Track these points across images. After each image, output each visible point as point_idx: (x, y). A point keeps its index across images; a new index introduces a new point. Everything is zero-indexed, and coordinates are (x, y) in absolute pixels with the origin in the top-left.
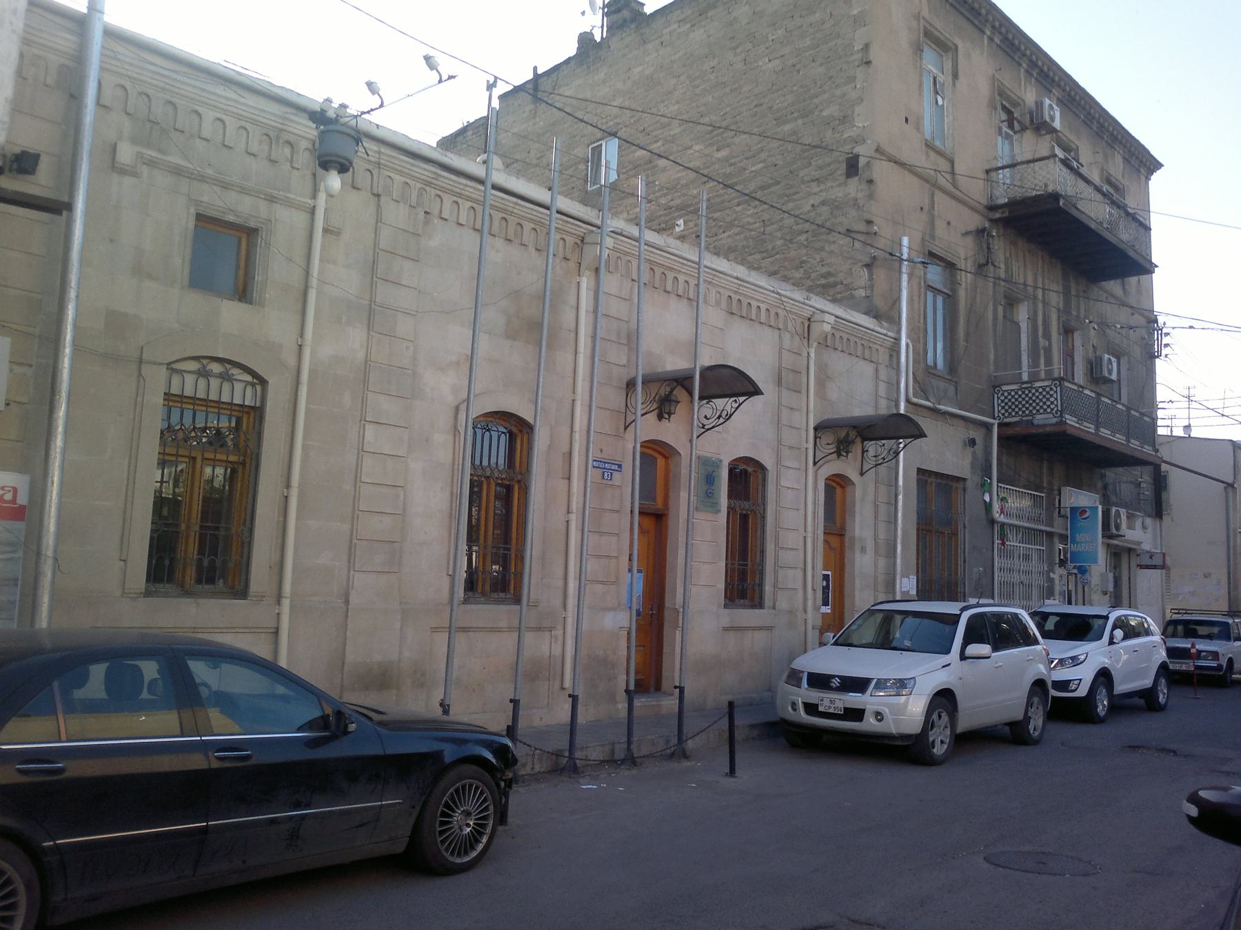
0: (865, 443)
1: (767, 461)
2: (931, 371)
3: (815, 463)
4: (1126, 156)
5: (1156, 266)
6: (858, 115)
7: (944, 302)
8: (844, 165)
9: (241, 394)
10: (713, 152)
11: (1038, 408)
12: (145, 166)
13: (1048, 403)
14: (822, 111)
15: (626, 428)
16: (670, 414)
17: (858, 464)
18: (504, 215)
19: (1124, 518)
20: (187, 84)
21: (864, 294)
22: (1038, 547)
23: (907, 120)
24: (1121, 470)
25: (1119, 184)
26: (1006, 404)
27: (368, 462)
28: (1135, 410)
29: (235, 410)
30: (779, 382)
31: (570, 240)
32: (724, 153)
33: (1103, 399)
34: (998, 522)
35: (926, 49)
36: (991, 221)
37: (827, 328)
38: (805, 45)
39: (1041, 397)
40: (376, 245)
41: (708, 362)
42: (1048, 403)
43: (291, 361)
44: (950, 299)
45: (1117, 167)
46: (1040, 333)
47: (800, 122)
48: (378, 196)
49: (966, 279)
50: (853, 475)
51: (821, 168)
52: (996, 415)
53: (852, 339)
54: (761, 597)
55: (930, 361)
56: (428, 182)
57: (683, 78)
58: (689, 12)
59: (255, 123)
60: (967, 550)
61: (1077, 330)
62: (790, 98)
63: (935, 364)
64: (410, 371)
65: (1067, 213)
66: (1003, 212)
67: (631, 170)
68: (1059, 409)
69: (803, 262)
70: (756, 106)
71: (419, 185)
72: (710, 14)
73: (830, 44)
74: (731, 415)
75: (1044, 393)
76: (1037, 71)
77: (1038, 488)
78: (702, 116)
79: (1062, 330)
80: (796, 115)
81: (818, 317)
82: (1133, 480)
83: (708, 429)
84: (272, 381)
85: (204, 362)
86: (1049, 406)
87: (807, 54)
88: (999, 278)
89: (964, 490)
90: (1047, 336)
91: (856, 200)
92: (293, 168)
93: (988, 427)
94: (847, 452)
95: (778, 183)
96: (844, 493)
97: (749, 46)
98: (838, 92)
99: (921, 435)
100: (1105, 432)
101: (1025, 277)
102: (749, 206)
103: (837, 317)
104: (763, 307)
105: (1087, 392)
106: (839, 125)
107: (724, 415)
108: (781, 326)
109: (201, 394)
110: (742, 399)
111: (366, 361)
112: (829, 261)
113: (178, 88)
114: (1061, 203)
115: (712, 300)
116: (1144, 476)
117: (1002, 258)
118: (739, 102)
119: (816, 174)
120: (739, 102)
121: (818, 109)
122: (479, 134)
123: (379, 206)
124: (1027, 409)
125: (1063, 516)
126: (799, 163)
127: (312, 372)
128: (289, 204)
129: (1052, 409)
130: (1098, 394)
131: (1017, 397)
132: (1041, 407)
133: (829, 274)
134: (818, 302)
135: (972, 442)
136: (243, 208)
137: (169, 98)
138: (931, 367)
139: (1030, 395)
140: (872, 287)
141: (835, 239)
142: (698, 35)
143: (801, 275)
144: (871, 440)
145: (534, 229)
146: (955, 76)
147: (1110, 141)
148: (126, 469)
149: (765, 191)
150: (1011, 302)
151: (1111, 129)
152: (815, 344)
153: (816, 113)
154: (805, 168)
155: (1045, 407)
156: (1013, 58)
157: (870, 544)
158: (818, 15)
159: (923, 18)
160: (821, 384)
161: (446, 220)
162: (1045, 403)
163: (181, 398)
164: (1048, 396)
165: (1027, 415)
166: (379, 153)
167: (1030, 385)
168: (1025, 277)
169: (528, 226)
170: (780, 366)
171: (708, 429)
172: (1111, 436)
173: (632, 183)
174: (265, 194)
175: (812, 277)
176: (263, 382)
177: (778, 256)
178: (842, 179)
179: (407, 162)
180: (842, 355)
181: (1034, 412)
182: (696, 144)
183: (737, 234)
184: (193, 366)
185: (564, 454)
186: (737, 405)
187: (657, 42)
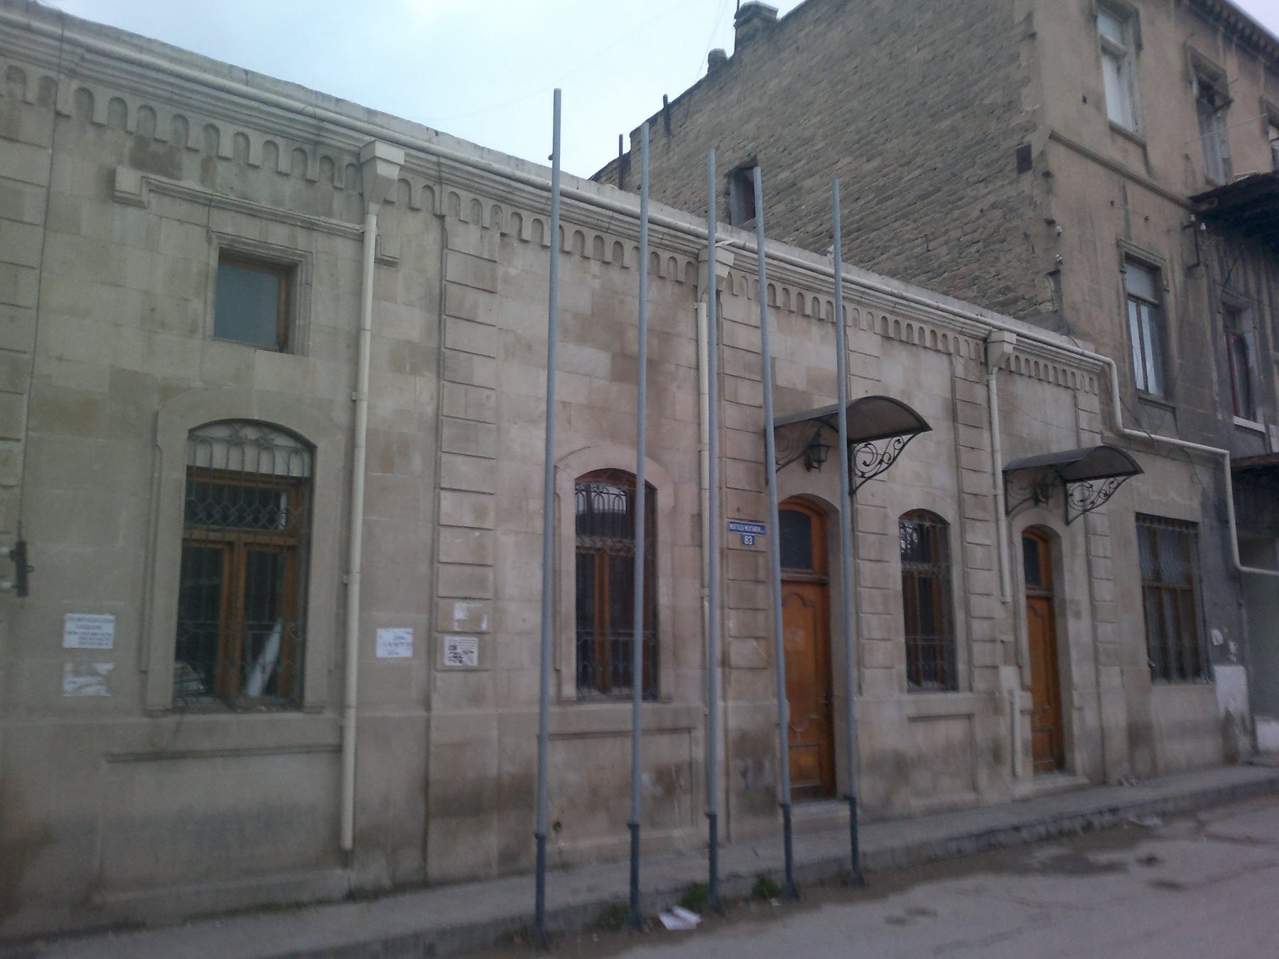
1: (949, 513)
2: (1143, 398)
3: (1007, 513)
6: (1026, 97)
7: (1150, 314)
9: (283, 464)
14: (982, 99)
16: (820, 462)
17: (1061, 512)
18: (598, 233)
21: (1051, 308)
23: (1085, 100)
30: (954, 416)
31: (682, 260)
32: (875, 163)
36: (1198, 215)
37: (1008, 349)
38: (959, 25)
40: (442, 277)
43: (341, 417)
44: (1157, 309)
47: (959, 115)
50: (1056, 525)
51: (987, 166)
53: (1042, 362)
55: (1140, 385)
56: (501, 196)
57: (823, 84)
58: (825, 8)
59: (283, 135)
63: (1146, 386)
64: (493, 426)
67: (774, 196)
69: (977, 278)
71: (492, 202)
74: (895, 459)
78: (847, 125)
80: (953, 108)
81: (996, 336)
83: (870, 478)
84: (322, 445)
91: (1033, 198)
92: (335, 188)
93: (1216, 461)
94: (1047, 498)
95: (939, 190)
99: (1136, 471)
101: (1246, 285)
102: (908, 220)
103: (1019, 335)
107: (886, 459)
110: (906, 438)
112: (1006, 273)
113: (179, 95)
115: (864, 325)
118: (888, 102)
120: (888, 102)
121: (979, 97)
122: (612, 179)
123: (443, 230)
128: (331, 232)
133: (1008, 289)
134: (995, 319)
136: (278, 238)
138: (1143, 392)
140: (1060, 298)
144: (1074, 481)
146: (1139, 46)
149: (926, 201)
150: (1233, 313)
152: (995, 370)
153: (977, 103)
154: (969, 168)
160: (1007, 415)
168: (1246, 285)
171: (870, 478)
173: (776, 211)
174: (303, 221)
175: (989, 294)
176: (310, 448)
177: (946, 275)
178: (1014, 175)
182: (843, 157)
183: (898, 254)
184: (222, 432)
186: (901, 445)
187: (794, 47)
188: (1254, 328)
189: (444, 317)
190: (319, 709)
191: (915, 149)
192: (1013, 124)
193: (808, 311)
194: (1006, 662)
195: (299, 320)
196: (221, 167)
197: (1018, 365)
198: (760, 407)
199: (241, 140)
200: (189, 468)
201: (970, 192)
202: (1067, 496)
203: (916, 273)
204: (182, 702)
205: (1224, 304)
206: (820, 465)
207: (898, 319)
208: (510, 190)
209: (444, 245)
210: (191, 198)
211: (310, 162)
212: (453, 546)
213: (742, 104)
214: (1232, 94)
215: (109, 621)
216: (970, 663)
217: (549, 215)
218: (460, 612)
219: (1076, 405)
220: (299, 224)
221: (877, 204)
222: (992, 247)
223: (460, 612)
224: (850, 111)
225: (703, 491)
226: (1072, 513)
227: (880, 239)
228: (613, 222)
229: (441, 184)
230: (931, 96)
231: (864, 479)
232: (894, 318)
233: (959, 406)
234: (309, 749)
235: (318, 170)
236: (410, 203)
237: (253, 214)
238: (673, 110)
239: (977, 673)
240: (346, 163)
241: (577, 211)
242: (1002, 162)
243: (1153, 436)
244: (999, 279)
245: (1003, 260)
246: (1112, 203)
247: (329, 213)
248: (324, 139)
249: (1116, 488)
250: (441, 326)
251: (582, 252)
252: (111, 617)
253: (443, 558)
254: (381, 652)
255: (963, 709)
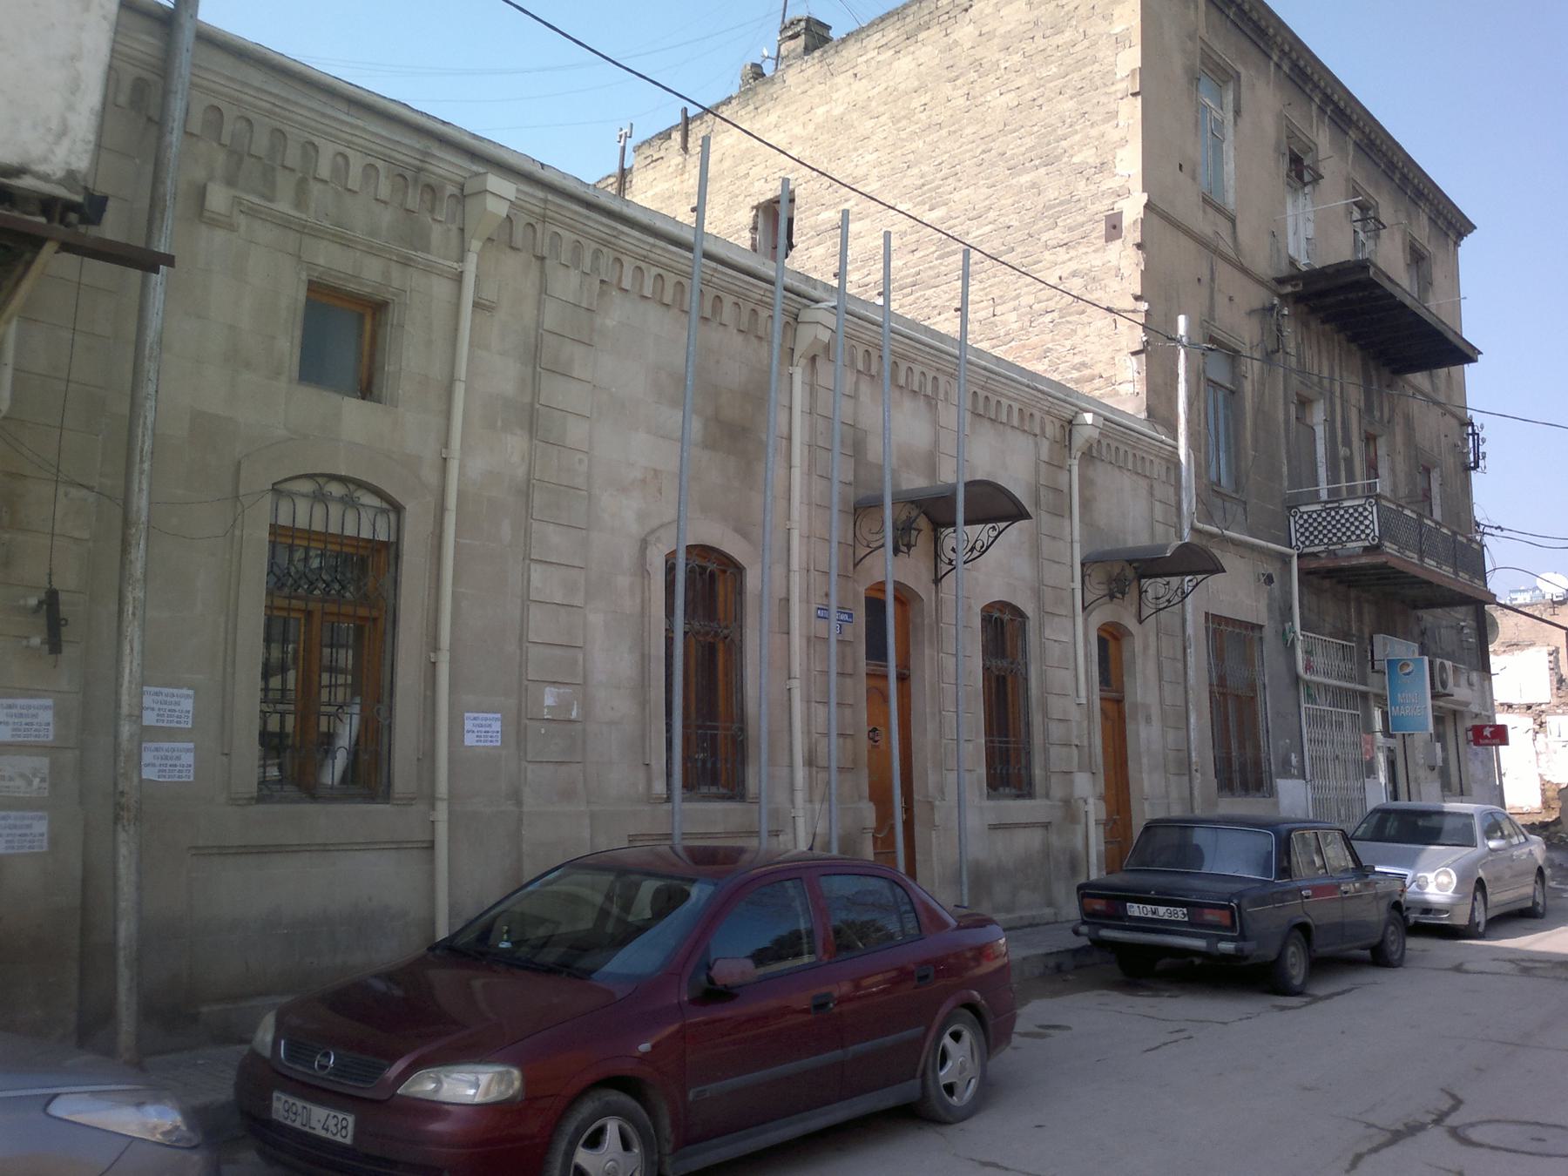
0: (1143, 581)
3: (1084, 608)
4: (1433, 216)
5: (1480, 353)
8: (1103, 225)
9: (366, 525)
10: (924, 212)
11: (1349, 533)
12: (242, 216)
13: (1362, 527)
14: (1072, 156)
15: (855, 565)
17: (1134, 609)
19: (1450, 672)
20: (303, 106)
22: (1354, 712)
24: (1439, 611)
25: (1426, 253)
26: (1307, 529)
27: (535, 614)
28: (1462, 535)
29: (346, 545)
33: (1426, 521)
34: (1304, 680)
35: (1204, 79)
36: (1280, 296)
39: (1352, 520)
40: (539, 324)
41: (968, 478)
42: (1362, 527)
43: (430, 475)
45: (1422, 231)
46: (1339, 439)
47: (1042, 170)
48: (542, 259)
49: (1252, 369)
50: (1130, 623)
51: (1071, 229)
52: (1294, 544)
54: (1030, 783)
57: (883, 119)
58: (893, 35)
59: (387, 159)
60: (1269, 715)
61: (1381, 436)
62: (1029, 141)
65: (1378, 286)
66: (1296, 285)
67: (812, 237)
68: (1377, 534)
69: (1049, 350)
70: (984, 152)
71: (594, 246)
72: (920, 37)
73: (1083, 71)
74: (988, 548)
75: (1356, 515)
76: (1332, 107)
77: (1346, 636)
79: (1363, 435)
82: (1454, 624)
84: (410, 507)
85: (321, 481)
86: (1363, 531)
87: (1051, 85)
88: (1291, 370)
89: (1261, 638)
90: (1347, 442)
93: (1285, 560)
95: (1013, 250)
96: (1120, 651)
97: (973, 75)
98: (1094, 132)
99: (1218, 569)
100: (1430, 563)
103: (1106, 419)
104: (1016, 406)
105: (1407, 512)
106: (1095, 173)
108: (1038, 431)
109: (318, 526)
110: (1002, 525)
111: (529, 481)
112: (1083, 348)
114: (1371, 273)
116: (1462, 615)
117: (1292, 345)
119: (1065, 237)
121: (1067, 155)
123: (542, 272)
124: (1335, 534)
125: (1377, 672)
126: (1041, 224)
127: (461, 495)
129: (1368, 535)
130: (1419, 515)
131: (1320, 520)
132: (1353, 533)
133: (1084, 365)
135: (1269, 579)
136: (370, 274)
137: (278, 125)
139: (1338, 517)
141: (1090, 320)
142: (905, 63)
143: (1045, 367)
144: (1150, 577)
145: (736, 304)
147: (1413, 196)
148: (531, 616)
150: (1304, 403)
151: (1416, 181)
155: (1358, 532)
156: (1304, 92)
157: (1155, 712)
158: (1067, 34)
159: (1201, 38)
160: (1086, 504)
161: (627, 291)
162: (1357, 527)
163: (293, 531)
164: (1361, 518)
165: (1334, 544)
166: (546, 201)
167: (1337, 505)
169: (728, 300)
170: (1037, 482)
172: (1437, 569)
175: (1061, 370)
176: (398, 509)
177: (1013, 343)
179: (580, 214)
180: (1109, 467)
181: (1344, 539)
184: (307, 487)
185: (780, 600)
186: (996, 533)
187: (851, 73)
188: (1326, 420)
189: (538, 369)
190: (410, 801)
191: (987, 202)
192: (1104, 187)
193: (902, 382)
194: (1081, 769)
195: (389, 365)
196: (315, 188)
197: (1099, 451)
198: (850, 484)
199: (340, 159)
200: (271, 525)
201: (1047, 255)
202: (1141, 592)
203: (979, 339)
204: (266, 792)
205: (1297, 394)
206: (909, 550)
207: (989, 395)
208: (615, 233)
209: (543, 289)
210: (285, 224)
211: (410, 191)
212: (541, 626)
213: (781, 130)
214: (1322, 171)
215: (188, 696)
216: (1046, 768)
217: (689, 276)
218: (550, 697)
219: (1152, 495)
220: (395, 258)
221: (937, 259)
222: (1068, 319)
223: (550, 697)
224: (913, 152)
225: (792, 574)
226: (1146, 612)
227: (939, 297)
228: (716, 274)
229: (544, 222)
230: (1011, 147)
231: (869, 550)
232: (985, 393)
233: (1043, 492)
234: (399, 846)
235: (418, 200)
236: (511, 241)
237: (346, 243)
238: (694, 124)
239: (1054, 779)
240: (448, 193)
241: (682, 261)
242: (1088, 227)
243: (1226, 532)
244: (1074, 354)
245: (1080, 333)
246: (1199, 280)
247: (427, 249)
248: (431, 167)
249: (1194, 587)
250: (535, 378)
251: (681, 304)
252: (191, 692)
253: (532, 638)
254: (470, 740)
255: (1042, 818)
